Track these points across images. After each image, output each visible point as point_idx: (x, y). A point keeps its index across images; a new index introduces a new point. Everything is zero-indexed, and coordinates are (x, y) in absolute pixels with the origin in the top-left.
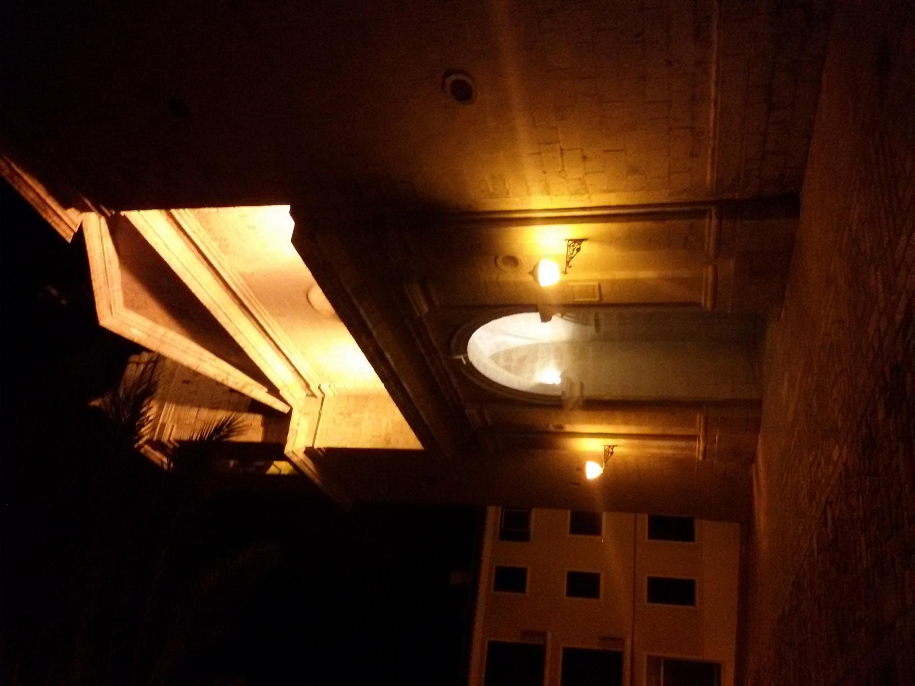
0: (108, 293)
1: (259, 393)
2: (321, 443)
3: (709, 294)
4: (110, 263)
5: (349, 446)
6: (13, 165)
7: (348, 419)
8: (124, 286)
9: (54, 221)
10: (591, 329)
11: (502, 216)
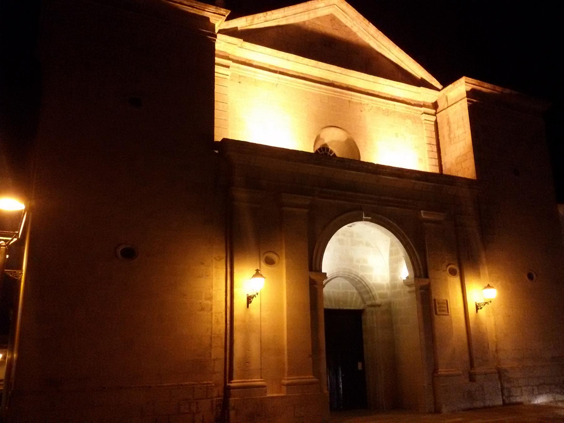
0: (357, 23)
4: (378, 46)
6: (496, 92)
8: (355, 34)
9: (474, 81)
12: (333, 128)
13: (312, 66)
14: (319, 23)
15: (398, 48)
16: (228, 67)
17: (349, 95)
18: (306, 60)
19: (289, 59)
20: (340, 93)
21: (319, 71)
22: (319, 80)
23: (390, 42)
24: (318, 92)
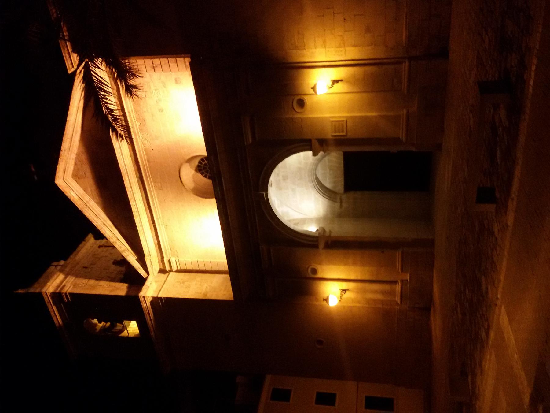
1: (132, 259)
2: (162, 295)
3: (404, 129)
4: (76, 133)
5: (180, 297)
7: (182, 285)
8: (78, 155)
10: (337, 205)
11: (300, 65)
12: (183, 180)
13: (135, 202)
14: (89, 190)
15: (68, 119)
16: (169, 261)
17: (143, 163)
18: (134, 209)
19: (140, 221)
20: (145, 172)
21: (135, 193)
22: (148, 210)
23: (67, 128)
24: (155, 192)
